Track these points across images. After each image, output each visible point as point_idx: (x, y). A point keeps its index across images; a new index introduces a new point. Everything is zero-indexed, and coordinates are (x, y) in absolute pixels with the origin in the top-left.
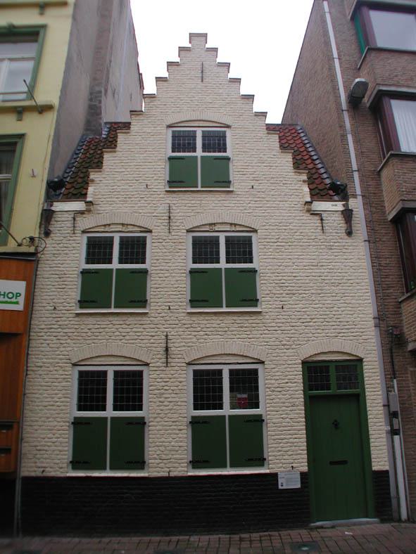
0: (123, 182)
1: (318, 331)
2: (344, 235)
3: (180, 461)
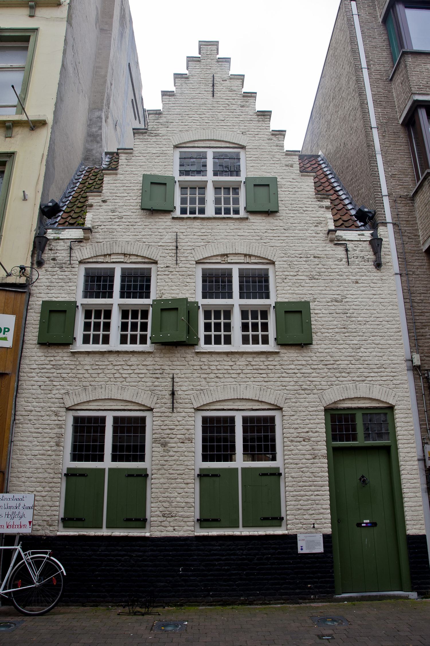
0: (125, 207)
1: (343, 374)
2: (372, 268)
3: (185, 519)
